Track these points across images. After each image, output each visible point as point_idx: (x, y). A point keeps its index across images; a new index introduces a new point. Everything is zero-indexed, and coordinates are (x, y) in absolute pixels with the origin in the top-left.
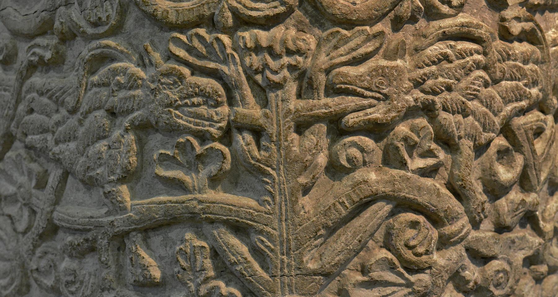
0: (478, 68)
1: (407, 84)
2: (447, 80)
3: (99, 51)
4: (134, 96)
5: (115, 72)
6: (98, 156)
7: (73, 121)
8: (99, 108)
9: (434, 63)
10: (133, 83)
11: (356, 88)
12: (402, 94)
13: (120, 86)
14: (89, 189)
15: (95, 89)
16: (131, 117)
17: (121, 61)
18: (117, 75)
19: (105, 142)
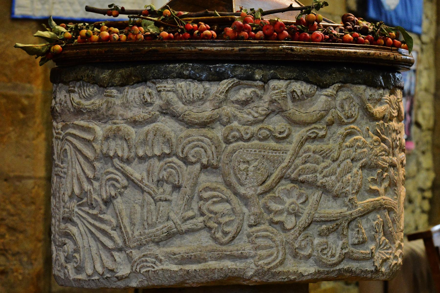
3: (350, 130)
4: (364, 152)
5: (357, 140)
6: (348, 182)
7: (335, 165)
8: (348, 158)
10: (364, 145)
13: (359, 147)
14: (335, 200)
15: (347, 149)
16: (361, 162)
17: (357, 135)
18: (357, 142)
19: (350, 175)
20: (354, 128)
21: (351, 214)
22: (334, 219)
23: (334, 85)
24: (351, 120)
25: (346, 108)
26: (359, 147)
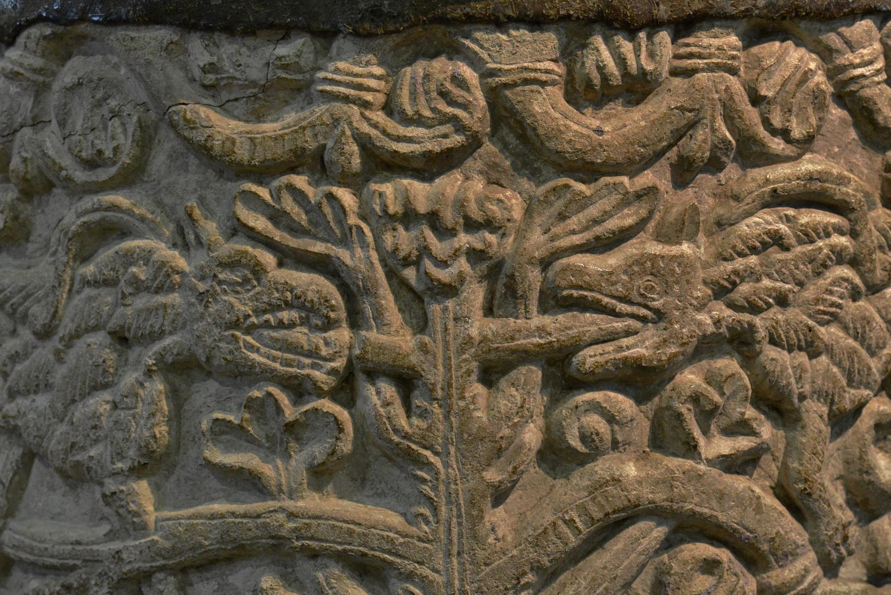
0: (840, 261)
1: (701, 291)
2: (779, 284)
3: (97, 216)
4: (165, 306)
5: (129, 259)
6: (92, 423)
7: (44, 353)
8: (95, 328)
9: (754, 250)
10: (163, 280)
11: (600, 297)
12: (690, 310)
13: (139, 287)
14: (73, 487)
15: (88, 291)
16: (157, 347)
17: (140, 236)
18: (132, 264)
19: (106, 395)
20: (114, 207)
21: (117, 555)
22: (55, 561)
23: (25, 34)
24: (103, 175)
25: (78, 122)
26: (139, 287)
